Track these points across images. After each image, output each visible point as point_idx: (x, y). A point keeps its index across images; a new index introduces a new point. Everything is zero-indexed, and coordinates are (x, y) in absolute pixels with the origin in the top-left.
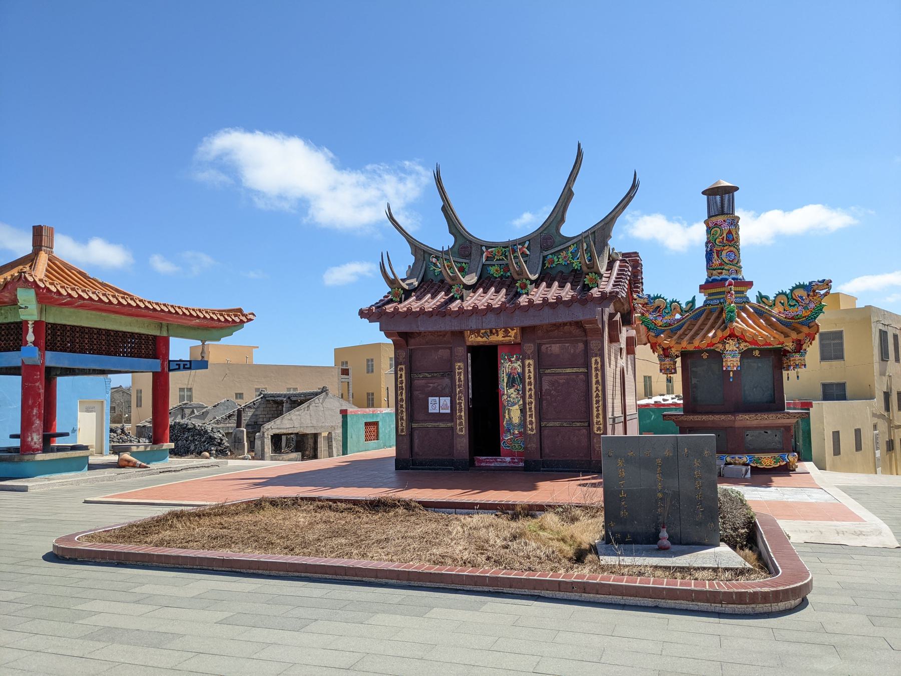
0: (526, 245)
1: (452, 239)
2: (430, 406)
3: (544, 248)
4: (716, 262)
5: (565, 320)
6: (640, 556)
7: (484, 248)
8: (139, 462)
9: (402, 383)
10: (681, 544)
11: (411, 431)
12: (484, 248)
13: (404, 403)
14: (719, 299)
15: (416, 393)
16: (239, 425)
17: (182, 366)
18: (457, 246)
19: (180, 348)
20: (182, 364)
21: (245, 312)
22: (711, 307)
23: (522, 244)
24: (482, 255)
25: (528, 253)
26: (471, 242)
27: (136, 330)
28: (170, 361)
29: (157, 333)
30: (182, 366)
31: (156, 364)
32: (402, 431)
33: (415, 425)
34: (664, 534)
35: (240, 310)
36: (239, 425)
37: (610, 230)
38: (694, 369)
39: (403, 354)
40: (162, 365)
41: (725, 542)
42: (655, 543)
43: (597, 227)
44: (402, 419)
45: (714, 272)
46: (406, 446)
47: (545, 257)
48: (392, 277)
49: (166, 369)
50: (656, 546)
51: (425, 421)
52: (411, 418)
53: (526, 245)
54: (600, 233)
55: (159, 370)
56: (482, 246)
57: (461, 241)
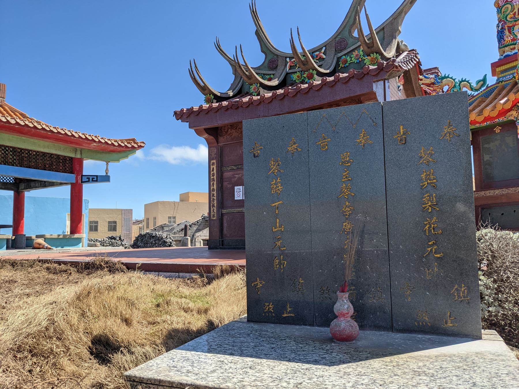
0: (323, 51)
1: (264, 56)
2: (236, 193)
3: (337, 51)
4: (508, 38)
5: (343, 97)
6: (282, 357)
7: (288, 60)
8: (46, 245)
9: (213, 176)
10: (391, 328)
11: (221, 217)
12: (288, 60)
13: (215, 193)
14: (513, 74)
15: (225, 184)
16: (186, 235)
17: (91, 180)
18: (267, 62)
19: (91, 166)
20: (91, 178)
21: (138, 141)
22: (504, 83)
23: (319, 50)
24: (286, 65)
25: (324, 57)
26: (277, 55)
27: (54, 152)
28: (82, 176)
29: (72, 155)
30: (91, 180)
31: (72, 178)
32: (214, 216)
33: (224, 211)
34: (344, 305)
35: (134, 140)
36: (186, 235)
37: (398, 25)
38: (486, 146)
39: (215, 150)
40: (77, 178)
41: (501, 332)
42: (326, 323)
43: (386, 23)
44: (213, 206)
45: (507, 49)
46: (216, 230)
47: (339, 59)
48: (202, 84)
49: (80, 181)
50: (325, 331)
51: (231, 207)
52: (221, 205)
53: (323, 51)
54: (389, 30)
55: (74, 182)
56: (286, 58)
57: (270, 57)
